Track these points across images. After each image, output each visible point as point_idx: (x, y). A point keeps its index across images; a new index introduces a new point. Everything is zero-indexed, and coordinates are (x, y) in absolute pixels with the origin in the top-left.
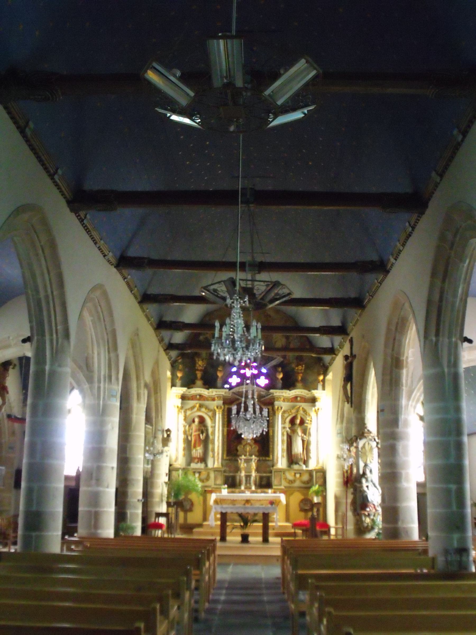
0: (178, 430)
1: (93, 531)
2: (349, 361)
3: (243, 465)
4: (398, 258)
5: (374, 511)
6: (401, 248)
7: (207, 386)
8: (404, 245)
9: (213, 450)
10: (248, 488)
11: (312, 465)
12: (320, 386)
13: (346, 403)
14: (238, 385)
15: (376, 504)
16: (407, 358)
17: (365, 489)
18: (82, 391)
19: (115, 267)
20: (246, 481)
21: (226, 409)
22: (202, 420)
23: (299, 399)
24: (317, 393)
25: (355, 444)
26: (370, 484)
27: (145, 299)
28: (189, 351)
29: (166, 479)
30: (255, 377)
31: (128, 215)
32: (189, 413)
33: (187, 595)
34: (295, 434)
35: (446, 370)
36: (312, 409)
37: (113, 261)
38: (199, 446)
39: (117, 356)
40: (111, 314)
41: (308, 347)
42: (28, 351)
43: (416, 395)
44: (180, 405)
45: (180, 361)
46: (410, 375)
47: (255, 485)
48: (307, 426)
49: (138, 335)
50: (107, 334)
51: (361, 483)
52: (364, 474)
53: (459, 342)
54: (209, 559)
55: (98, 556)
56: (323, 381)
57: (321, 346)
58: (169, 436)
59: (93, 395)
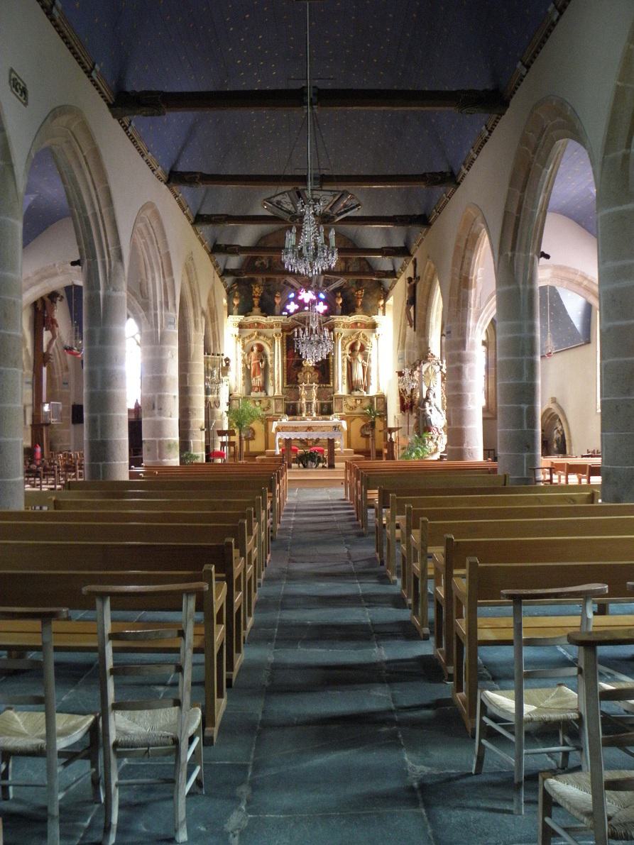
0: (237, 360)
1: (158, 460)
2: (412, 283)
3: (303, 393)
4: (470, 167)
5: (437, 434)
6: (475, 156)
7: (264, 314)
8: (478, 153)
9: (273, 379)
10: (310, 415)
11: (373, 392)
12: (380, 312)
13: (409, 327)
14: (296, 311)
15: (440, 428)
16: (476, 277)
17: (428, 412)
18: (138, 320)
19: (165, 184)
20: (307, 408)
21: (285, 337)
22: (261, 349)
23: (359, 324)
24: (378, 318)
25: (418, 369)
26: (433, 409)
27: (199, 220)
28: (246, 277)
29: (227, 408)
30: (313, 303)
31: (176, 120)
32: (247, 341)
33: (263, 514)
34: (356, 360)
35: (521, 286)
36: (372, 335)
37: (164, 177)
38: (259, 374)
39: (173, 281)
40: (164, 235)
41: (367, 270)
42: (77, 278)
43: (484, 316)
44: (237, 334)
45: (236, 288)
46: (478, 296)
47: (316, 412)
48: (367, 353)
49: (192, 259)
50: (161, 257)
51: (424, 407)
52: (427, 398)
53: (536, 258)
54: (279, 483)
55: (161, 482)
56: (384, 306)
57: (382, 269)
58: (227, 365)
59: (149, 322)
